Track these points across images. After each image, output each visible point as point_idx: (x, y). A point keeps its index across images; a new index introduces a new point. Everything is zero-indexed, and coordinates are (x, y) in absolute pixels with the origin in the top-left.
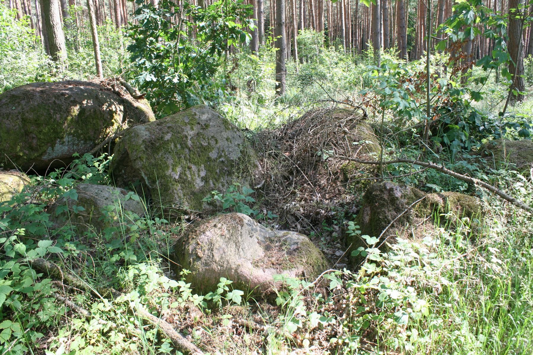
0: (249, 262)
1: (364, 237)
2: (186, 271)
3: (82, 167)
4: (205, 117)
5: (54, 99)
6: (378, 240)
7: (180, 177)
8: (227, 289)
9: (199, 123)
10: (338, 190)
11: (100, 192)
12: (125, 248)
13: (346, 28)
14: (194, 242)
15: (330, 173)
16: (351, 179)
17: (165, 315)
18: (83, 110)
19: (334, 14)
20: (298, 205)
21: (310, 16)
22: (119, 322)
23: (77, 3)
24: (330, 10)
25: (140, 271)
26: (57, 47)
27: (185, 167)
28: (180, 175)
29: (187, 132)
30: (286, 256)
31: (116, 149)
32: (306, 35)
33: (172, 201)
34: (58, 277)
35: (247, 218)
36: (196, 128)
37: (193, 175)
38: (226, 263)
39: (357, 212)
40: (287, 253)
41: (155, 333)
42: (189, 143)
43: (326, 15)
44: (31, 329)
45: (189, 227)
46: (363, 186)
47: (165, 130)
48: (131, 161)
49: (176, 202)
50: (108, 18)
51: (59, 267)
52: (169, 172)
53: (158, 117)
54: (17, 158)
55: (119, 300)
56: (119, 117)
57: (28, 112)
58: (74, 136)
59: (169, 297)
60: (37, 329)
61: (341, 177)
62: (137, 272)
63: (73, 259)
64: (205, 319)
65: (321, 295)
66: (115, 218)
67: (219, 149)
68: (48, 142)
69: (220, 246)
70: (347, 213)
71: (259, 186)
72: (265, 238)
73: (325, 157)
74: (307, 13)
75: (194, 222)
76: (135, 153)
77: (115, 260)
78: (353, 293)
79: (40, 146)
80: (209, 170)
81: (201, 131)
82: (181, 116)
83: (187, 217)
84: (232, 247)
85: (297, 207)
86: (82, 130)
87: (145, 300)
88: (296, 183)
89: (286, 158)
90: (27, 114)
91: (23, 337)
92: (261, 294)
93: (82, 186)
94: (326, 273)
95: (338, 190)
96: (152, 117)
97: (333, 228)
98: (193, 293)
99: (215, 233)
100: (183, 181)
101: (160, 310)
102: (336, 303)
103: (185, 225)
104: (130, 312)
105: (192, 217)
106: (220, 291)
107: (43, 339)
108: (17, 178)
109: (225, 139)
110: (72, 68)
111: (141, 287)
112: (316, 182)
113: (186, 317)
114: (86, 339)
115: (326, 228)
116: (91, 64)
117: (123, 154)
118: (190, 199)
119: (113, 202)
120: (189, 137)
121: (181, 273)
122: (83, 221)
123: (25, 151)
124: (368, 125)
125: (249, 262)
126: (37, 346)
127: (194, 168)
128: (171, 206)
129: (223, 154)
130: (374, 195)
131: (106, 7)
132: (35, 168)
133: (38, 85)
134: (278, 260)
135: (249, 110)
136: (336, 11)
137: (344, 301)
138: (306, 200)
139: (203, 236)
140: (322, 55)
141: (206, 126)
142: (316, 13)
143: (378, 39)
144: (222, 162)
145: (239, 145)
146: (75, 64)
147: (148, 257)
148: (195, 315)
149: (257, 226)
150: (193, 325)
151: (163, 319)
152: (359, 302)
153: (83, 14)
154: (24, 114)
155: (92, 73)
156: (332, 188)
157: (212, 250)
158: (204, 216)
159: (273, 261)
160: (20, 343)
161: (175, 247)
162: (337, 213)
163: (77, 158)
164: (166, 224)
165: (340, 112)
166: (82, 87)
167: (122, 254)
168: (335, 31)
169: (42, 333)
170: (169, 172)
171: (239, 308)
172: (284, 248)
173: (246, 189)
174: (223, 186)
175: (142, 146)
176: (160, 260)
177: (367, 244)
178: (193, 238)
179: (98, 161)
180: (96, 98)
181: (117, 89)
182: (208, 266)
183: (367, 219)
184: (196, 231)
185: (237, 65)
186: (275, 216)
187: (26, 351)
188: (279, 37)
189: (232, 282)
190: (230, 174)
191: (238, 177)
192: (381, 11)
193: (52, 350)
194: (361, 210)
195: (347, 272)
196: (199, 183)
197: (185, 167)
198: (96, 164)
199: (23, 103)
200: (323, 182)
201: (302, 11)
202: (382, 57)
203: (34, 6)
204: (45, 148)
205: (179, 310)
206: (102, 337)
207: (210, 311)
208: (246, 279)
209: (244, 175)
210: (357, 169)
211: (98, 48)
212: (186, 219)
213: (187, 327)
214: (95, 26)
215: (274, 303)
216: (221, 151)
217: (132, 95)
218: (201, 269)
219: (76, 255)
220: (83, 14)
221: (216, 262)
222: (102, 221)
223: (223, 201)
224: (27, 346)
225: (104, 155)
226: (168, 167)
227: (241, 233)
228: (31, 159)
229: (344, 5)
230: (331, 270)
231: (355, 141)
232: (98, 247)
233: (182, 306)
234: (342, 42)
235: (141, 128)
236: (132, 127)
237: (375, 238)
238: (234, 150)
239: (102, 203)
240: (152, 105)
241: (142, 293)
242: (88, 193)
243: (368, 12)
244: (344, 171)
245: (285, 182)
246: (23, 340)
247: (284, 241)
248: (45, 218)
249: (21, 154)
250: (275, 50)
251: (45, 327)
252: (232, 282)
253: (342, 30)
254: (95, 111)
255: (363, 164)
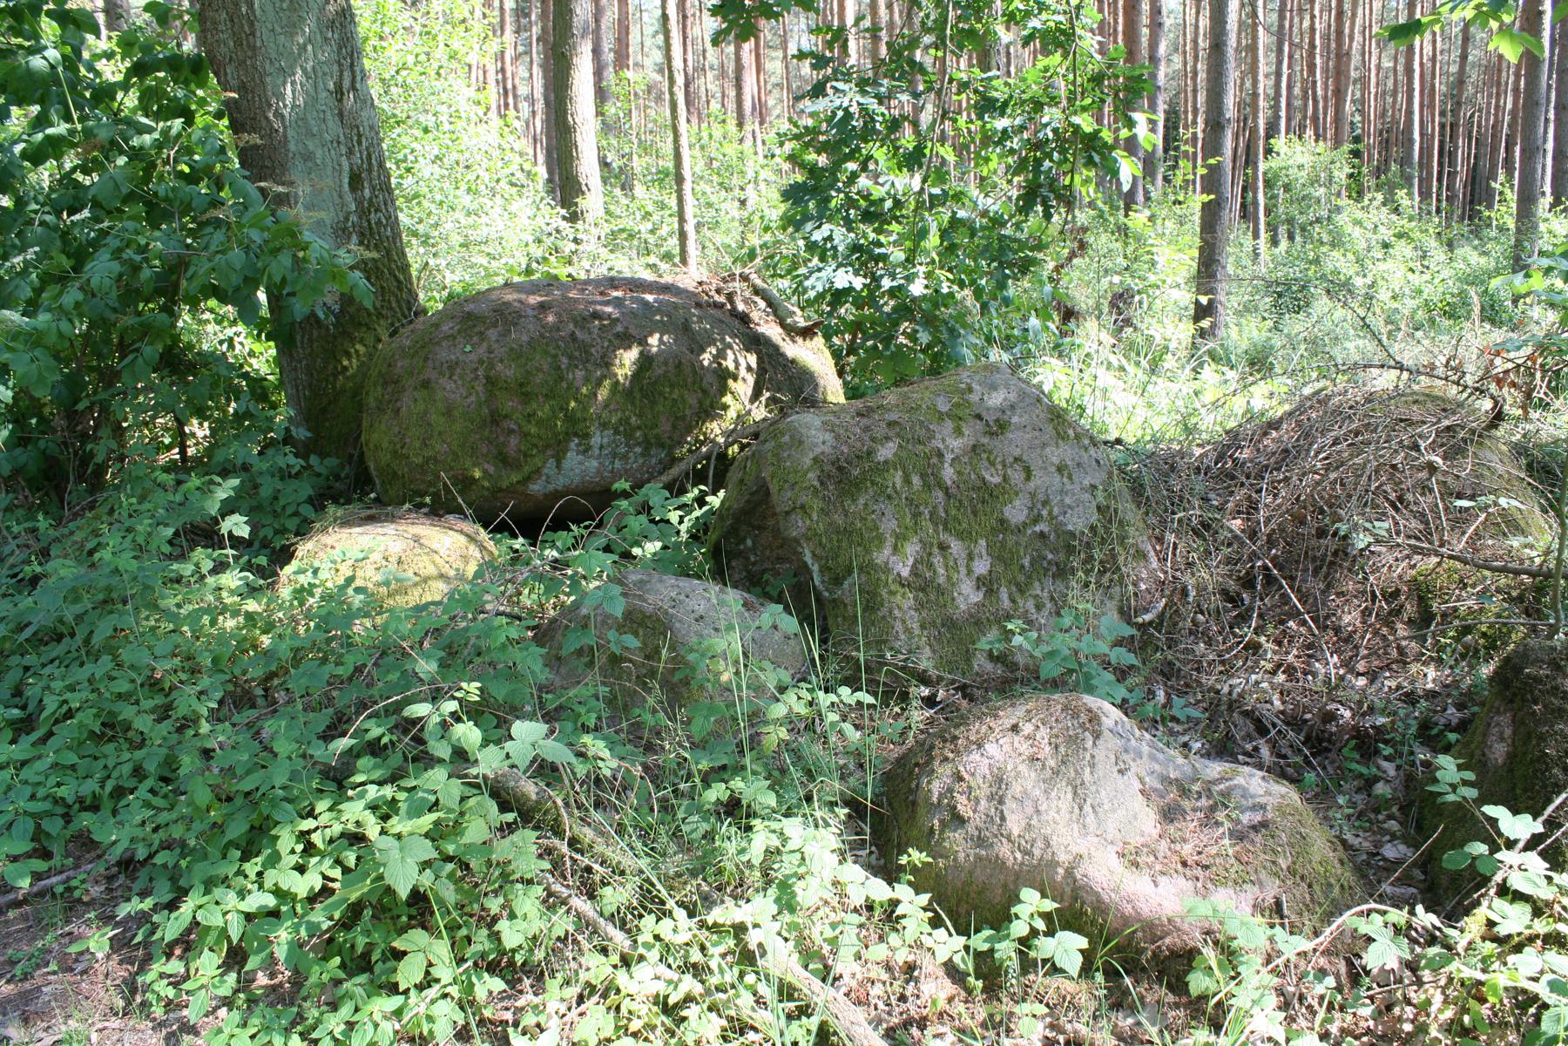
0: (1112, 849)
1: (1490, 810)
2: (917, 856)
3: (637, 523)
4: (996, 399)
5: (571, 326)
6: (1538, 828)
7: (914, 572)
8: (1040, 925)
9: (979, 417)
10: (1399, 647)
11: (682, 597)
12: (743, 768)
13: (1422, 135)
14: (949, 772)
15: (1373, 593)
16: (1444, 615)
17: (846, 979)
18: (645, 361)
19: (1384, 93)
20: (1264, 685)
21: (1305, 98)
22: (714, 980)
23: (636, 64)
24: (1373, 80)
25: (785, 840)
26: (580, 184)
27: (932, 545)
28: (914, 565)
29: (943, 440)
30: (1226, 841)
31: (733, 475)
32: (1295, 155)
33: (885, 642)
34: (558, 832)
35: (1112, 715)
36: (971, 432)
37: (951, 567)
38: (1040, 844)
39: (1462, 727)
40: (1232, 833)
41: (814, 1029)
42: (948, 473)
43: (1358, 94)
44: (476, 964)
45: (931, 722)
46: (1482, 641)
47: (880, 430)
48: (775, 514)
49: (897, 645)
50: (715, 106)
51: (559, 802)
52: (883, 555)
53: (852, 392)
54: (466, 483)
55: (716, 915)
56: (743, 387)
57: (501, 361)
58: (617, 432)
59: (861, 926)
60: (489, 964)
61: (1410, 609)
62: (775, 842)
63: (598, 781)
64: (961, 1008)
65: (1330, 981)
66: (725, 678)
67: (1033, 495)
68: (548, 446)
69: (1025, 792)
70: (1425, 726)
71: (1148, 617)
72: (1165, 780)
73: (1361, 541)
74: (1297, 91)
75: (947, 708)
76: (789, 494)
77: (713, 799)
78: (1444, 989)
79: (525, 456)
80: (1002, 556)
81: (985, 440)
82: (927, 394)
83: (925, 692)
84: (1062, 799)
85: (1265, 692)
86: (640, 416)
87: (792, 926)
88: (1260, 616)
89: (1236, 537)
90: (499, 367)
91: (455, 981)
92: (1142, 951)
93: (633, 577)
94: (1361, 914)
95: (1399, 647)
96: (833, 389)
97: (1378, 768)
98: (936, 923)
99: (1015, 750)
100: (921, 583)
101: (830, 962)
102: (1380, 1013)
103: (918, 715)
104: (747, 958)
105: (941, 694)
106: (1019, 929)
107: (503, 996)
108: (463, 539)
109: (1053, 469)
110: (613, 241)
111: (784, 886)
112: (1327, 617)
113: (908, 993)
114: (617, 1018)
115: (1354, 766)
116: (664, 231)
117: (752, 494)
118: (939, 640)
119: (716, 630)
120: (949, 457)
121: (904, 860)
122: (634, 678)
123: (486, 466)
124: (1504, 448)
125: (1112, 849)
126: (487, 1013)
127: (956, 547)
128: (883, 656)
129: (1045, 513)
130: (1528, 675)
131: (710, 75)
132: (523, 518)
133: (534, 288)
134: (1199, 853)
135: (1121, 383)
136: (1390, 83)
137: (1409, 1012)
138: (1290, 671)
139: (975, 756)
140: (1341, 219)
141: (1000, 427)
142: (1326, 85)
143: (1535, 169)
144: (1042, 535)
145: (1094, 487)
146: (623, 230)
147: (809, 799)
148: (935, 990)
149: (1143, 741)
150: (925, 1019)
151: (838, 989)
152: (1461, 1021)
153: (649, 92)
154: (491, 366)
155: (667, 257)
156: (1378, 640)
157: (1001, 802)
158: (978, 693)
159: (1183, 853)
160: (445, 996)
161: (887, 778)
162: (1393, 722)
163: (625, 495)
164: (870, 706)
165: (1415, 402)
166: (650, 298)
167: (737, 784)
168: (1386, 145)
169: (503, 978)
170: (883, 555)
171: (1070, 987)
172: (1220, 816)
173: (1111, 623)
174: (1039, 607)
175: (810, 475)
176: (843, 812)
177: (1500, 834)
178: (946, 759)
179: (678, 508)
180: (684, 329)
181: (741, 307)
182: (986, 848)
183: (1499, 752)
184: (955, 738)
185: (1083, 246)
186: (1195, 713)
187: (461, 1022)
188: (1212, 161)
189: (1056, 905)
190: (1062, 572)
191: (1087, 585)
192: (1550, 77)
193: (524, 1033)
194: (1477, 722)
195: (1426, 919)
196: (968, 596)
197: (932, 545)
198: (674, 517)
199: (492, 334)
200: (1350, 618)
201: (1284, 85)
202: (1542, 227)
203: (527, 75)
204: (538, 461)
205: (889, 968)
206: (663, 1018)
207: (980, 984)
208: (1099, 900)
209: (1105, 580)
210: (1465, 585)
211: (687, 186)
212: (923, 699)
213: (907, 1024)
214: (683, 127)
215: (1178, 986)
216: (1039, 504)
217: (783, 325)
218: (961, 855)
219: (608, 773)
220: (649, 92)
221: (1009, 840)
222: (686, 682)
223: (1037, 653)
224: (462, 1008)
225: (696, 491)
226: (880, 540)
227: (1093, 757)
228: (501, 490)
229: (1422, 64)
230: (1373, 905)
231: (1460, 496)
232: (670, 752)
233: (902, 956)
234: (1408, 181)
235: (808, 423)
236: (785, 415)
237: (1528, 817)
238: (1079, 502)
239: (685, 627)
240: (837, 355)
241: (787, 903)
242: (651, 598)
243: (1499, 84)
244: (1421, 591)
245: (1227, 611)
246: (454, 991)
247: (1222, 794)
248: (533, 662)
249: (477, 474)
250: (1197, 200)
251: (511, 963)
252: (1056, 905)
253: (1411, 141)
254: (679, 365)
255: (1487, 573)
